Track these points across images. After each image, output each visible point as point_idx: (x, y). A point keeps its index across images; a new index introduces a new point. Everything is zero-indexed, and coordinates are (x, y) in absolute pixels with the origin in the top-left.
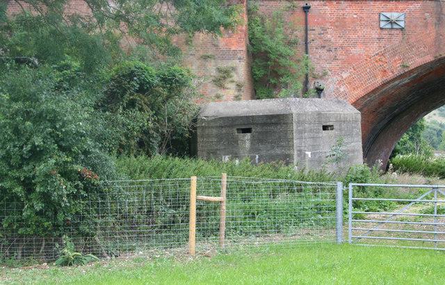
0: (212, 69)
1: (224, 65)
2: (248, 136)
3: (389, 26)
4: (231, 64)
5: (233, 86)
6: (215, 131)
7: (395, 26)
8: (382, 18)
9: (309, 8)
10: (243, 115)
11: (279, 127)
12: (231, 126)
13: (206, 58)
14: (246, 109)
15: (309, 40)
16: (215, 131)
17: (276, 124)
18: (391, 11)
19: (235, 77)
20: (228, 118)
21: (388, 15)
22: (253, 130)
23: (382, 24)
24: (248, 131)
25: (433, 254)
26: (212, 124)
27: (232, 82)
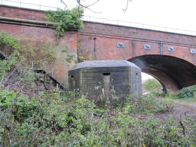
0: (65, 55)
1: (70, 54)
2: (108, 77)
3: (120, 47)
4: (73, 54)
5: (74, 62)
6: (91, 74)
7: (121, 47)
8: (118, 44)
9: (96, 38)
10: (105, 67)
11: (124, 72)
12: (100, 72)
13: (64, 51)
14: (106, 64)
15: (96, 49)
16: (91, 74)
17: (123, 71)
18: (120, 42)
19: (74, 59)
20: (98, 68)
21: (119, 43)
22: (111, 74)
23: (118, 46)
24: (107, 74)
25: (82, 117)
26: (90, 71)
27: (73, 60)
